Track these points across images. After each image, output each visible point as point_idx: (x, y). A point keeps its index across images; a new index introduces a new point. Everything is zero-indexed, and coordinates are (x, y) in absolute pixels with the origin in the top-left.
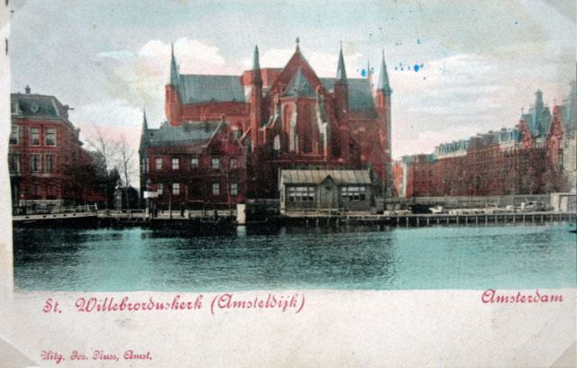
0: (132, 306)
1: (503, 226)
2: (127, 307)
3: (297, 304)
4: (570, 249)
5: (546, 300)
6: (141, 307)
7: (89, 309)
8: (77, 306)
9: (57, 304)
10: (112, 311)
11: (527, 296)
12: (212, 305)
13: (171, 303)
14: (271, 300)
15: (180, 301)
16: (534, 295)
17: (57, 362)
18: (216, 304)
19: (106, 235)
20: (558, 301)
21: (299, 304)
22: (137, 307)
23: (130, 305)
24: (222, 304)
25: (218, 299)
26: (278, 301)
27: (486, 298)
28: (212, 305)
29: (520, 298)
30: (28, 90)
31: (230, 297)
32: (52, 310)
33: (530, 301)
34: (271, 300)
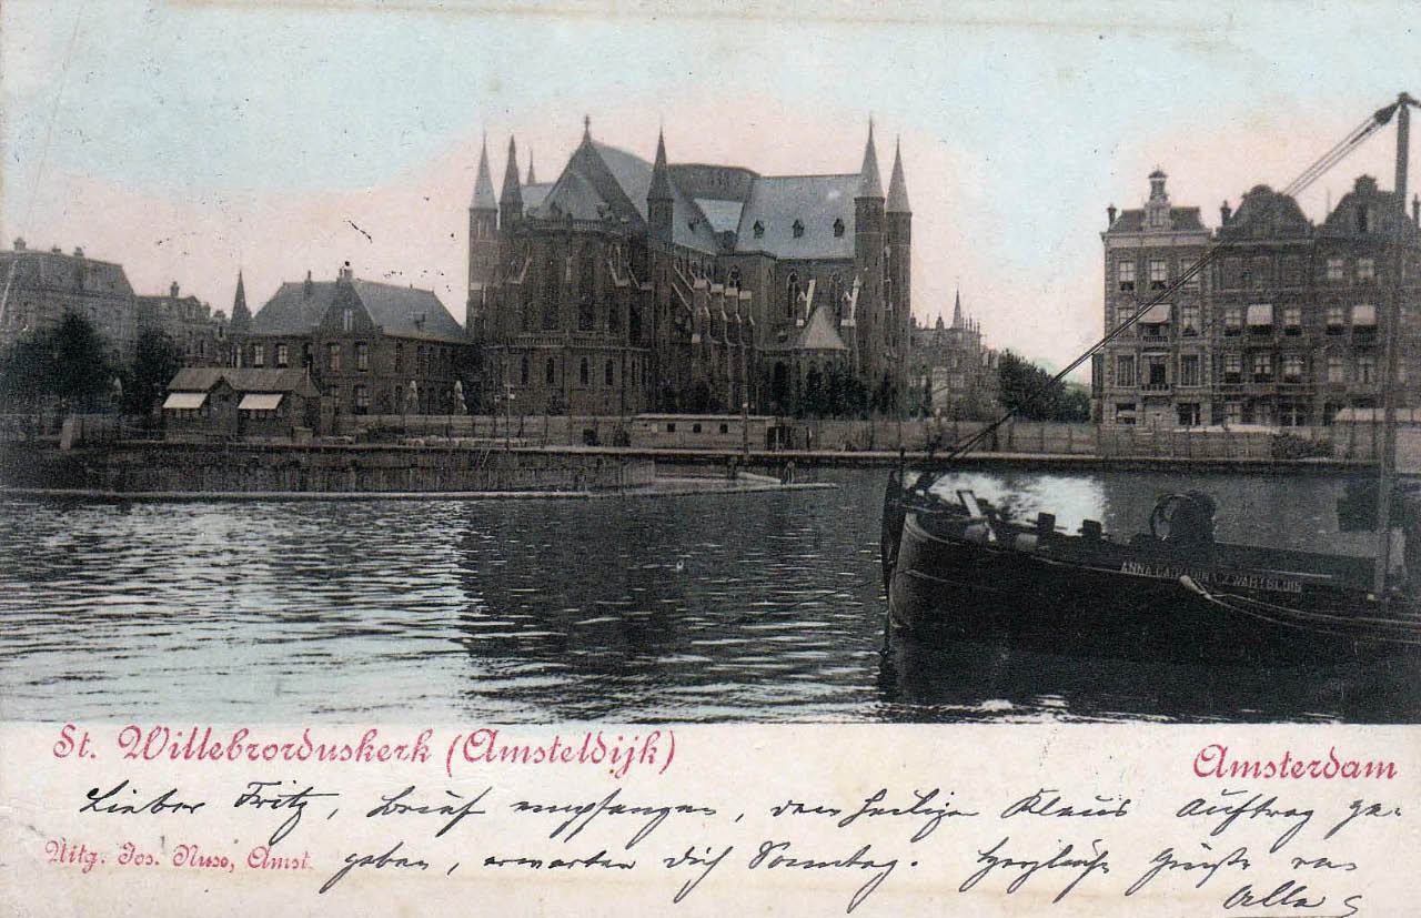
0: (259, 751)
1: (344, 291)
2: (245, 754)
3: (657, 757)
4: (30, 272)
5: (1354, 775)
6: (280, 754)
7: (232, 756)
8: (122, 745)
9: (86, 740)
10: (559, 761)
11: (1306, 763)
12: (451, 752)
13: (355, 747)
14: (593, 743)
15: (378, 743)
16: (298, 741)
17: (775, 815)
18: (459, 748)
19: (535, 642)
20: (1384, 776)
21: (661, 757)
22: (270, 753)
23: (253, 747)
24: (473, 752)
25: (460, 744)
26: (610, 749)
27: (1204, 767)
28: (451, 752)
29: (1289, 766)
30: (175, 289)
31: (494, 735)
32: (1278, 774)
33: (1314, 776)
34: (593, 743)
